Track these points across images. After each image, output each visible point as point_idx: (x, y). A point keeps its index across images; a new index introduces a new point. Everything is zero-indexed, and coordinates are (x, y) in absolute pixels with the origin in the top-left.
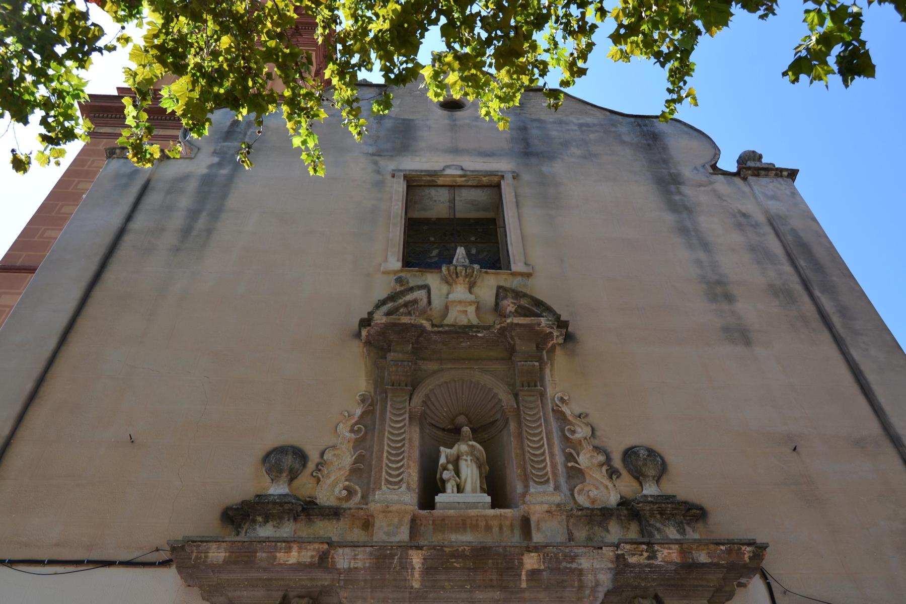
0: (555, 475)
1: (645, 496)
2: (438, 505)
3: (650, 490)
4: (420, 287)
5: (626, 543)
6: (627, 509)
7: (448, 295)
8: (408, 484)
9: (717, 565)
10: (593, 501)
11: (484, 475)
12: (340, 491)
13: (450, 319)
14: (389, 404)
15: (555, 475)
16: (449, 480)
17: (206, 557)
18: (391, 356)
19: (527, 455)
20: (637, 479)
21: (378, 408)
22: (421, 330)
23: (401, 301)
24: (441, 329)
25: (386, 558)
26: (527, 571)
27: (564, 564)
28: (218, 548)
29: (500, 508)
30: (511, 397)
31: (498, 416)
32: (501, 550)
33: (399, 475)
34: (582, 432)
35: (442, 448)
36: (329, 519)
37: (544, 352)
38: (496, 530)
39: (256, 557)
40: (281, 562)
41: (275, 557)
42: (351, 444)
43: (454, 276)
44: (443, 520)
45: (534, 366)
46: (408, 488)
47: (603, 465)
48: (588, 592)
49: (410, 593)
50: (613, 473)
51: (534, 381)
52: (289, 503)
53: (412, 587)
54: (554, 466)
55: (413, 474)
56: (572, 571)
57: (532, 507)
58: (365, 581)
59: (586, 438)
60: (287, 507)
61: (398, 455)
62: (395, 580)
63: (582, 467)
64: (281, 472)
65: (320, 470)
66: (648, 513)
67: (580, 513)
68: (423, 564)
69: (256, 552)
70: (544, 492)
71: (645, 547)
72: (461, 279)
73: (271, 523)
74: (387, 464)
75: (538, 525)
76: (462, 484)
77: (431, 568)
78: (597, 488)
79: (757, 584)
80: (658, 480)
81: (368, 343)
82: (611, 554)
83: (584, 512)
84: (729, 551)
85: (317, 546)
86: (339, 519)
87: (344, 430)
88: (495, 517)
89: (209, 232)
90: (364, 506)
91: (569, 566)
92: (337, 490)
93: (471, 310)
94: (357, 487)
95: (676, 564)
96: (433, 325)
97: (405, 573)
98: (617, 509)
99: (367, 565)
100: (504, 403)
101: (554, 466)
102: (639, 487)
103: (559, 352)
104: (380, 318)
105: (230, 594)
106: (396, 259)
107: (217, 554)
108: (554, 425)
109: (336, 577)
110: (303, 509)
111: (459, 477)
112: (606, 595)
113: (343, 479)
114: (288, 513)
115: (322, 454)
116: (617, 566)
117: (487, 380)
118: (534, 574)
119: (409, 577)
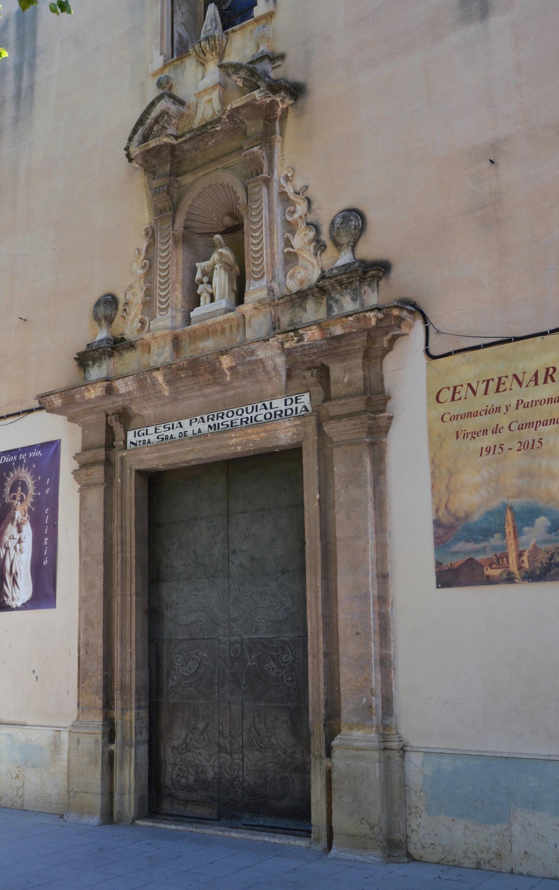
16: (202, 292)
17: (53, 404)
22: (173, 148)
24: (184, 139)
26: (227, 369)
35: (197, 264)
36: (131, 350)
38: (228, 331)
39: (75, 398)
43: (202, 56)
44: (194, 332)
56: (256, 361)
59: (301, 217)
60: (100, 350)
62: (155, 393)
67: (282, 301)
71: (292, 334)
75: (250, 321)
80: (354, 246)
82: (276, 343)
83: (285, 299)
84: (358, 320)
85: (100, 384)
89: (32, 87)
91: (250, 359)
96: (176, 137)
99: (135, 387)
103: (291, 115)
106: (159, 53)
108: (278, 210)
113: (140, 312)
114: (104, 354)
118: (231, 369)
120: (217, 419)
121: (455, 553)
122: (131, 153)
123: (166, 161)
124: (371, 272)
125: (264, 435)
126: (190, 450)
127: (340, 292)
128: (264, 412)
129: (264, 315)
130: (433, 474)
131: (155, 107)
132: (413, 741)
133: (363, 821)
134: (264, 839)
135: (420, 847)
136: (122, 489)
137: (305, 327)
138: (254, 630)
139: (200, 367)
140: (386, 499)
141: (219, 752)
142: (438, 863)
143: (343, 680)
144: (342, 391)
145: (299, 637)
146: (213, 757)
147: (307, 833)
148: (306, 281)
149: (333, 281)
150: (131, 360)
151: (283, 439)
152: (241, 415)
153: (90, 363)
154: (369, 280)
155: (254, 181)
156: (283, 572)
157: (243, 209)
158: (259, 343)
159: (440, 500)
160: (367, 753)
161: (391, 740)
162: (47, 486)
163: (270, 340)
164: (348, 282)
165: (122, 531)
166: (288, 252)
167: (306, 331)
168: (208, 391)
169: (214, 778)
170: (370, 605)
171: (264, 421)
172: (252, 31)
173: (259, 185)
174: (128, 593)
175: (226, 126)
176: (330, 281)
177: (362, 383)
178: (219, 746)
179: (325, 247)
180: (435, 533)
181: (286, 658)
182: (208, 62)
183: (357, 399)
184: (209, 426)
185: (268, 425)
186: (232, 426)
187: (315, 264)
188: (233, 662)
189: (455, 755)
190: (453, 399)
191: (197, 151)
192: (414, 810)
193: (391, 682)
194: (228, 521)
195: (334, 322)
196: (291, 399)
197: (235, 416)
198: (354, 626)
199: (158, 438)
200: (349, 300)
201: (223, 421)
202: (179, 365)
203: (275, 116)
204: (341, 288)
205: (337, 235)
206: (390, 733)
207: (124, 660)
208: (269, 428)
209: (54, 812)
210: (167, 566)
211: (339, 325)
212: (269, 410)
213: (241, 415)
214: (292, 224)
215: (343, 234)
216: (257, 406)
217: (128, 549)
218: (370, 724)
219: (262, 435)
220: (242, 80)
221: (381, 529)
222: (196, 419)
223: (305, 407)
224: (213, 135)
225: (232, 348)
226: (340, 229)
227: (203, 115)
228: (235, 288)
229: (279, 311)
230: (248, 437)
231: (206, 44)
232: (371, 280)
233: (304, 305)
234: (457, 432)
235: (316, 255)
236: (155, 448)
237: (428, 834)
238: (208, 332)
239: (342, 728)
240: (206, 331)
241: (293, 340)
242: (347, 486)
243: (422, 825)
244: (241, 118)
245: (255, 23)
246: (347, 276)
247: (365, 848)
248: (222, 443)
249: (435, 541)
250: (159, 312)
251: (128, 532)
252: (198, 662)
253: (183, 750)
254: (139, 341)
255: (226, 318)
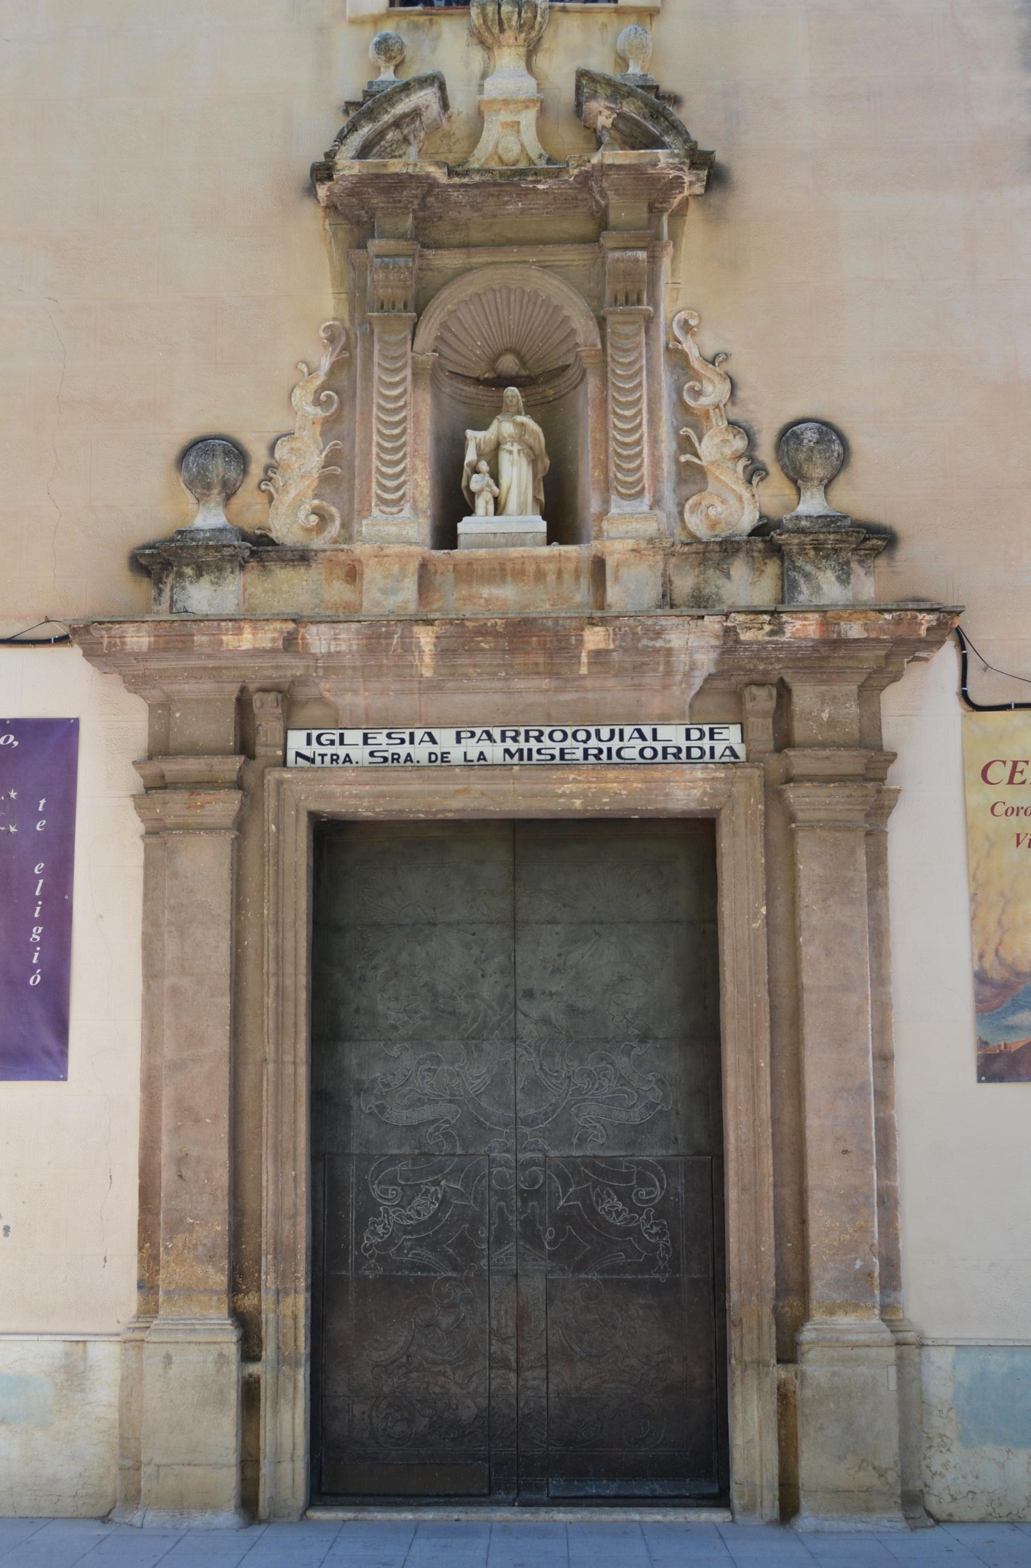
0: (656, 478)
1: (798, 518)
2: (462, 540)
3: (812, 504)
4: (423, 82)
5: (738, 612)
6: (765, 542)
7: (484, 76)
8: (415, 501)
9: (877, 640)
10: (713, 525)
11: (540, 476)
12: (307, 516)
13: (481, 156)
14: (377, 348)
15: (656, 478)
16: (481, 491)
17: (123, 643)
18: (375, 245)
19: (612, 444)
20: (795, 482)
21: (359, 352)
22: (429, 185)
23: (386, 118)
24: (466, 180)
25: (382, 637)
27: (645, 642)
28: (138, 631)
29: (562, 542)
30: (592, 325)
31: (571, 360)
32: (550, 623)
33: (398, 488)
34: (714, 391)
35: (469, 433)
37: (665, 218)
38: (551, 578)
39: (193, 642)
40: (231, 648)
41: (221, 642)
42: (318, 428)
43: (496, 30)
44: (470, 564)
45: (637, 261)
46: (415, 509)
47: (740, 457)
48: (678, 678)
49: (420, 682)
50: (755, 472)
51: (630, 296)
52: (229, 546)
53: (422, 676)
54: (656, 461)
55: (421, 484)
56: (657, 651)
57: (608, 543)
58: (354, 668)
59: (717, 407)
60: (227, 552)
61: (396, 450)
63: (704, 463)
64: (209, 487)
65: (270, 479)
66: (795, 549)
67: (686, 549)
68: (435, 645)
69: (193, 635)
70: (632, 515)
72: (509, 34)
73: (206, 578)
74: (378, 468)
76: (503, 497)
77: (447, 650)
78: (723, 502)
79: (948, 655)
80: (828, 484)
81: (331, 208)
84: (898, 622)
85: (278, 625)
86: (309, 566)
87: (302, 399)
88: (550, 559)
90: (345, 547)
91: (651, 643)
92: (302, 515)
93: (528, 119)
94: (333, 510)
95: (813, 640)
96: (451, 173)
97: (410, 658)
98: (748, 542)
100: (580, 339)
101: (656, 461)
102: (795, 497)
103: (694, 215)
104: (349, 166)
105: (165, 688)
107: (137, 639)
109: (312, 663)
110: (253, 553)
111: (497, 484)
112: (706, 681)
113: (310, 493)
114: (231, 561)
115: (272, 449)
116: (724, 644)
117: (551, 287)
118: (599, 656)
119: (417, 662)
120: (527, 740)
121: (1011, 1029)
122: (339, 167)
123: (406, 208)
124: (874, 541)
125: (639, 786)
126: (458, 791)
127: (814, 562)
128: (639, 744)
129: (650, 566)
130: (973, 897)
131: (407, 96)
132: (933, 1332)
133: (865, 1465)
134: (630, 1517)
135: (948, 1498)
136: (277, 846)
137: (796, 612)
138: (575, 1141)
139: (531, 636)
140: (887, 929)
141: (490, 1368)
142: (982, 1521)
143: (814, 1230)
144: (816, 734)
145: (675, 1156)
146: (473, 1379)
147: (721, 1499)
148: (723, 524)
149: (808, 539)
150: (292, 588)
151: (678, 800)
152: (585, 742)
153: (189, 571)
154: (862, 552)
155: (623, 313)
156: (643, 1039)
157: (588, 357)
158: (681, 618)
159: (987, 941)
160: (873, 1352)
161: (901, 1328)
162: (39, 816)
163: (706, 618)
164: (833, 549)
165: (277, 931)
166: (688, 463)
167: (797, 619)
168: (519, 684)
169: (477, 1416)
170: (870, 1103)
171: (640, 760)
172: (604, 25)
173: (633, 323)
174: (288, 1058)
175: (559, 188)
176: (803, 538)
177: (855, 727)
178: (491, 1357)
179: (767, 474)
180: (977, 994)
181: (648, 1194)
182: (500, 46)
183: (855, 753)
184: (507, 751)
185: (656, 770)
186: (562, 758)
187: (744, 498)
188: (525, 1201)
189: (1011, 1349)
190: (1011, 782)
191: (476, 211)
192: (937, 1440)
193: (897, 1234)
194: (514, 935)
195: (851, 615)
196: (700, 730)
197: (570, 742)
198: (838, 1139)
199: (372, 754)
200: (833, 579)
201: (540, 745)
202: (485, 624)
203: (664, 205)
204: (817, 555)
205: (806, 460)
206: (894, 1317)
207: (280, 1193)
208: (658, 775)
209: (69, 1515)
210: (357, 1011)
211: (860, 622)
212: (650, 742)
213: (585, 742)
214: (692, 414)
215: (819, 461)
216: (621, 732)
217: (289, 969)
218: (869, 1304)
219: (635, 785)
220: (615, 115)
221: (881, 979)
222: (473, 735)
223: (731, 749)
224: (526, 195)
225: (618, 617)
226: (815, 452)
227: (497, 146)
228: (542, 497)
229: (671, 566)
230: (603, 785)
231: (513, 12)
232: (866, 555)
233: (725, 566)
234: (1018, 835)
235: (751, 483)
236: (374, 774)
237: (964, 1477)
238: (503, 569)
239: (814, 1312)
240: (497, 567)
241: (762, 629)
242: (825, 900)
243: (952, 1464)
244: (605, 185)
245: (614, 15)
246: (838, 537)
247: (869, 1510)
248: (538, 787)
249: (977, 1007)
250: (377, 505)
251: (290, 935)
252: (437, 1199)
253: (399, 1367)
254: (328, 553)
255: (556, 553)
